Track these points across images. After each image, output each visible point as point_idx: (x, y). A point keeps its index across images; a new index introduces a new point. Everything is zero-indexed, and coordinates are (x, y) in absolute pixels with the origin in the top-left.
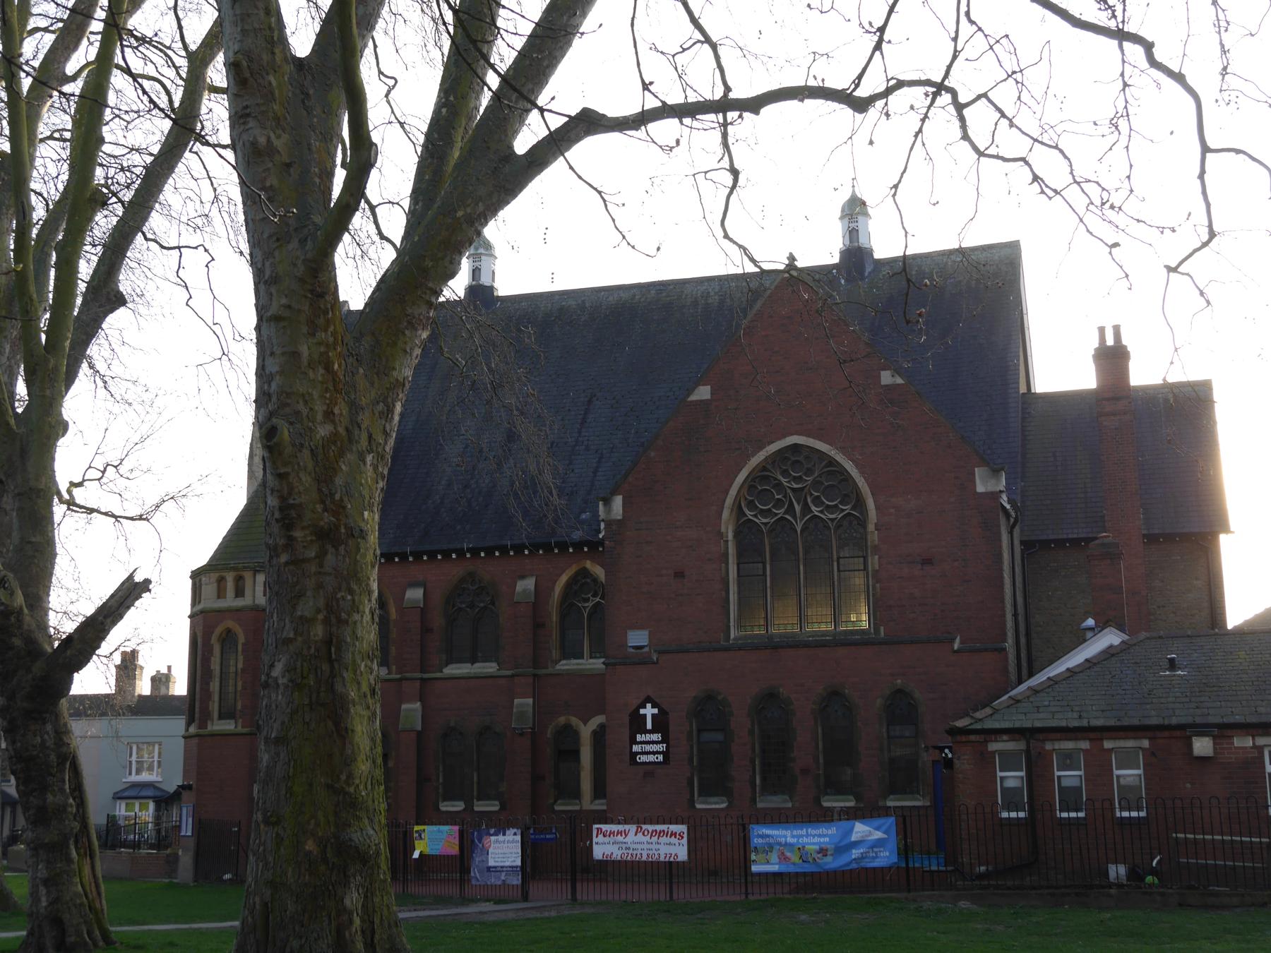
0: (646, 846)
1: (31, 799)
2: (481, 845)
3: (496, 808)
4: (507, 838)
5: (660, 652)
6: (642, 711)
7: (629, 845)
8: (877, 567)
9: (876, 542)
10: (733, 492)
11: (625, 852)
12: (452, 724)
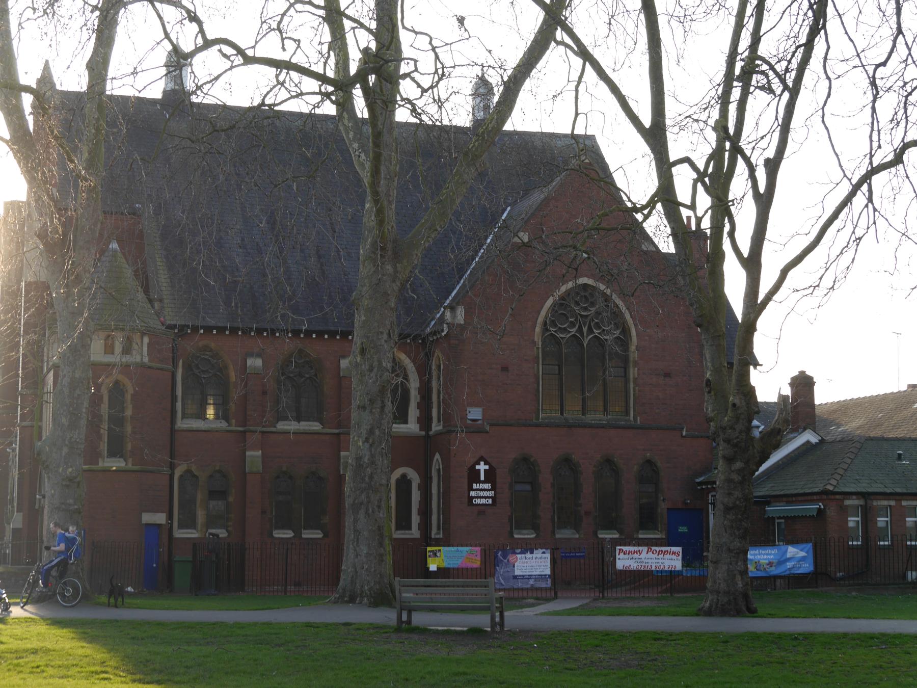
0: (654, 561)
1: (743, 523)
2: (506, 561)
3: (320, 536)
4: (534, 555)
5: (491, 425)
6: (477, 467)
7: (643, 560)
8: (636, 376)
9: (637, 359)
10: (543, 313)
11: (640, 564)
12: (284, 469)
